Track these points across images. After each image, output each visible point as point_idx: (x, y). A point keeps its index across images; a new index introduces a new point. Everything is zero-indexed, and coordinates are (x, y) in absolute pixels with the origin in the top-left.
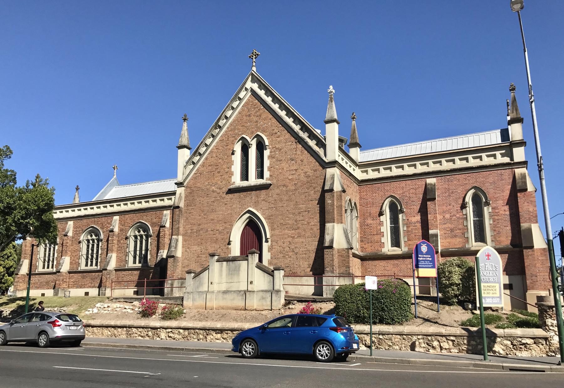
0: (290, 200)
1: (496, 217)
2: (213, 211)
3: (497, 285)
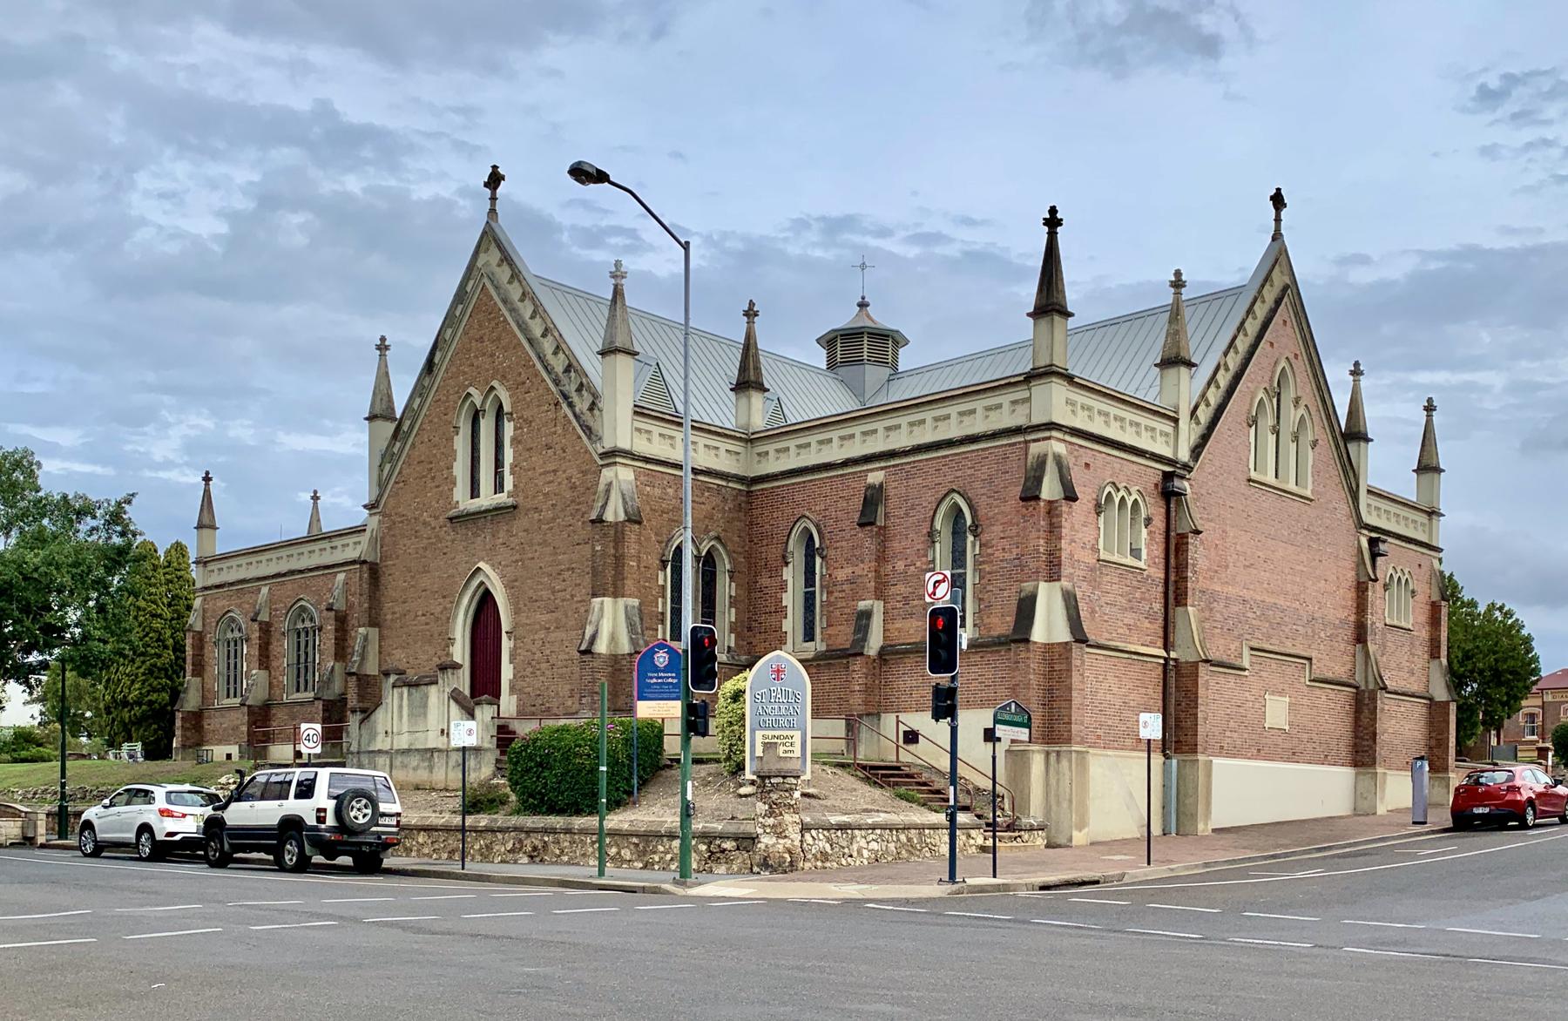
0: (544, 543)
1: (987, 568)
2: (426, 570)
3: (797, 735)
